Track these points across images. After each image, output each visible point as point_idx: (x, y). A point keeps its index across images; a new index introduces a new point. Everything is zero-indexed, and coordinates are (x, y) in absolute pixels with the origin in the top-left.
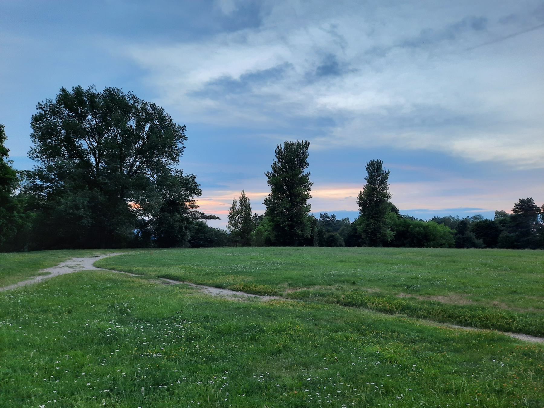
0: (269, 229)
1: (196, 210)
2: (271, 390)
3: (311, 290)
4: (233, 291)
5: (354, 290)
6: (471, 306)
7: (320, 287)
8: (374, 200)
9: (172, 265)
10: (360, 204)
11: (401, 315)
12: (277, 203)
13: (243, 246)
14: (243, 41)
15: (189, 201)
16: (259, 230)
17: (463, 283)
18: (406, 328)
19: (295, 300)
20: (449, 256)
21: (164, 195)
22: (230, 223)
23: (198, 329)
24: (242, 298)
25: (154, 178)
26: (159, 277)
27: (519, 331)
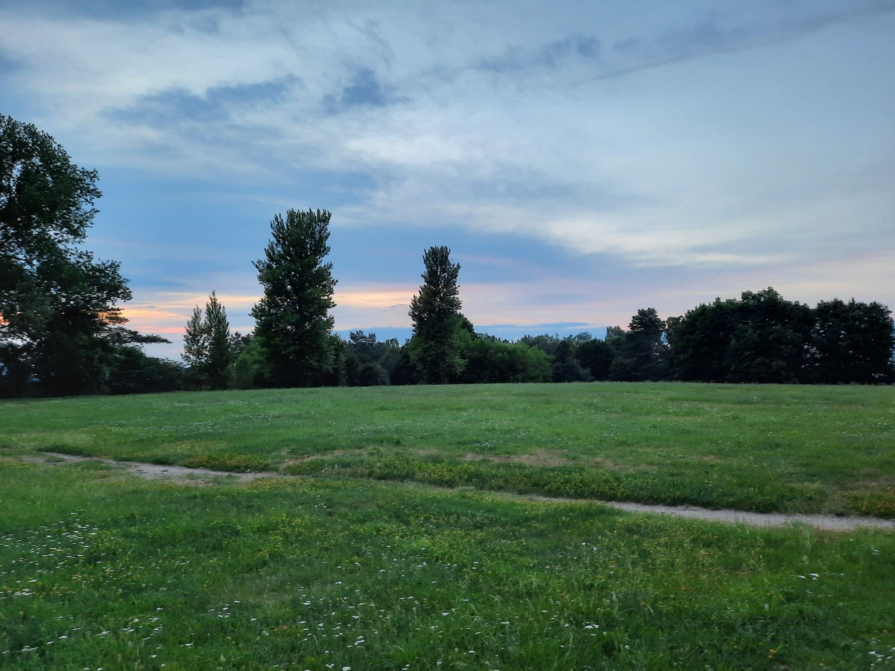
0: (261, 358)
1: (121, 325)
2: (242, 630)
3: (328, 457)
4: (189, 467)
5: (397, 454)
6: (565, 467)
7: (342, 452)
8: (436, 309)
9: (71, 427)
10: (414, 316)
11: (466, 488)
12: (276, 314)
13: (213, 388)
14: (212, 28)
15: (107, 309)
16: (244, 362)
17: (558, 434)
18: (470, 506)
19: (298, 477)
20: (542, 395)
21: (55, 298)
22: (189, 350)
23: (111, 539)
24: (203, 479)
25: (33, 266)
26: (40, 450)
27: (626, 499)
